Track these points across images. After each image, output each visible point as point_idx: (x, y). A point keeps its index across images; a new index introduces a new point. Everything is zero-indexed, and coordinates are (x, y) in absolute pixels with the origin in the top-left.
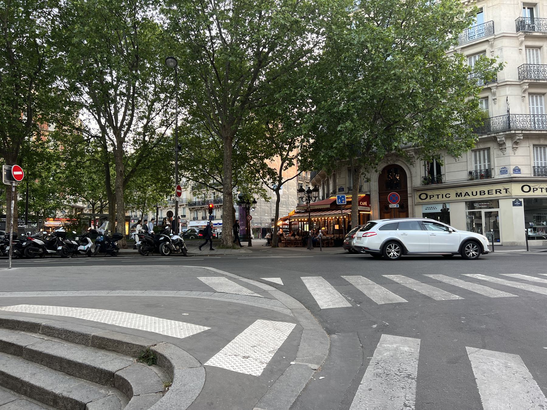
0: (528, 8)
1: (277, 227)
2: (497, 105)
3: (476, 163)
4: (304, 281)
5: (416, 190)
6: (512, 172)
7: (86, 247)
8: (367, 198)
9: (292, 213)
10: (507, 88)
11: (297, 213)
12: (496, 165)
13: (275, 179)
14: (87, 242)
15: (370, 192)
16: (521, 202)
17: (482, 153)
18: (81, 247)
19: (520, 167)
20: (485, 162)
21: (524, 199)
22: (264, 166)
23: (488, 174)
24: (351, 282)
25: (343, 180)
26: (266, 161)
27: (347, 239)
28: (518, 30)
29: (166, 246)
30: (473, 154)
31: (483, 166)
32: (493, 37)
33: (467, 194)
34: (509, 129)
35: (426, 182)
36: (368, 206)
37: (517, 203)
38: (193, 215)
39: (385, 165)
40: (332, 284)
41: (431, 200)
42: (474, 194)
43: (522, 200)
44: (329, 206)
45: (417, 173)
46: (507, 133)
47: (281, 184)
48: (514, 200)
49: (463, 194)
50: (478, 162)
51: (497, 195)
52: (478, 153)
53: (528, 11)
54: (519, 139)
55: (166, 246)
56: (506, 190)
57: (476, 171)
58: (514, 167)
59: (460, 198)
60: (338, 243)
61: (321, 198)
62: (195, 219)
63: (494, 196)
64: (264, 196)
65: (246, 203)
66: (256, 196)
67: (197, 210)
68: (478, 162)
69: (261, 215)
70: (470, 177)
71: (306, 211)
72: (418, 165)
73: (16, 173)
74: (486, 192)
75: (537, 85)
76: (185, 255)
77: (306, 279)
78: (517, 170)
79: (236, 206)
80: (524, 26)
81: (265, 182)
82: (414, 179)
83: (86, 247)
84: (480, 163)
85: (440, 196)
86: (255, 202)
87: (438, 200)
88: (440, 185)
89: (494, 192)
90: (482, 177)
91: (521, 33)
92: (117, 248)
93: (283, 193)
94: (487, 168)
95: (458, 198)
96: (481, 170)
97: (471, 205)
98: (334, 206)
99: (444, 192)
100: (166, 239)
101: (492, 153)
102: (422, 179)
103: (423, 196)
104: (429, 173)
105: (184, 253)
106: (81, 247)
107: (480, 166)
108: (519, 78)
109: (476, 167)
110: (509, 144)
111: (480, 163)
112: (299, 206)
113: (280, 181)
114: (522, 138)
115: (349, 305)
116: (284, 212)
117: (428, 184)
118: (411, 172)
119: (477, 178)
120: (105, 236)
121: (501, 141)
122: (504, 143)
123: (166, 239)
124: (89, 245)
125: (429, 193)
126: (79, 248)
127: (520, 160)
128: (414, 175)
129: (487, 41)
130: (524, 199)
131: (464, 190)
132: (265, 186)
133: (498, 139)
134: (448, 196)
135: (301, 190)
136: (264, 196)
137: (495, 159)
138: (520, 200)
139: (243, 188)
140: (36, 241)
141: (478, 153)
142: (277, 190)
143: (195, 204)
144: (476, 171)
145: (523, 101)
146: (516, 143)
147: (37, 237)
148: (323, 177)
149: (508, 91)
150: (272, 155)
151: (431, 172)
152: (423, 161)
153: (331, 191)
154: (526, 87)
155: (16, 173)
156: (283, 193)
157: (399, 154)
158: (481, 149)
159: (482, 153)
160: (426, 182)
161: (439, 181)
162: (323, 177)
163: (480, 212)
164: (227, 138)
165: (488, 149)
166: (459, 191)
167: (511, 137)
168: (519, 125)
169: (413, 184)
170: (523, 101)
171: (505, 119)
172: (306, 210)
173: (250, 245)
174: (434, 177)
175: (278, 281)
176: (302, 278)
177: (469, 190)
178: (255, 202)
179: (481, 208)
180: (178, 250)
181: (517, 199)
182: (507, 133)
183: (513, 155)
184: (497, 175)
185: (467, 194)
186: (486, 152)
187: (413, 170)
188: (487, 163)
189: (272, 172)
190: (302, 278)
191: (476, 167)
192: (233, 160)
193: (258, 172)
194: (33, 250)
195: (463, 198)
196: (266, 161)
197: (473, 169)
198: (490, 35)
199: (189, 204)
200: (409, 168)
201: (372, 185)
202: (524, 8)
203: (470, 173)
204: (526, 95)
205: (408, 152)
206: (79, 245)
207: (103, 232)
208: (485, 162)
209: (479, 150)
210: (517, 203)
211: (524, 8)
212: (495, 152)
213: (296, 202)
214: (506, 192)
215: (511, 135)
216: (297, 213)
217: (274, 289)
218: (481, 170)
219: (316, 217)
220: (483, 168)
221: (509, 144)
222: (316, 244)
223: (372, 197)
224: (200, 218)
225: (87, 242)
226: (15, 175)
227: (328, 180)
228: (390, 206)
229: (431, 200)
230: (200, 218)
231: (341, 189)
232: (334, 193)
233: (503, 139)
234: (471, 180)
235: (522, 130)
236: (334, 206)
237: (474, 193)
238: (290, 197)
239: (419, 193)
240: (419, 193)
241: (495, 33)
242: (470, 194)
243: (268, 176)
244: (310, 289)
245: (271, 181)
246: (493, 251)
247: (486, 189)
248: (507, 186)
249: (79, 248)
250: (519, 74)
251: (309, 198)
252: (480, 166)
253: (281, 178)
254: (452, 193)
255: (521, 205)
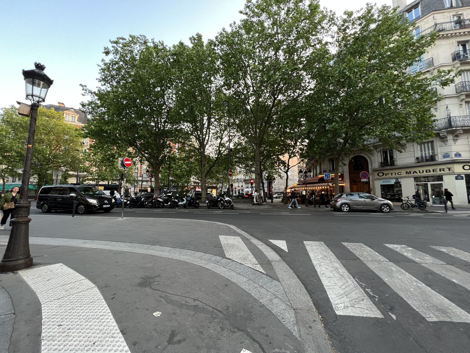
0: (462, 45)
1: (286, 192)
2: (438, 112)
3: (421, 151)
4: (308, 248)
5: (375, 170)
6: (454, 156)
7: (183, 203)
8: (342, 176)
9: (295, 185)
10: (447, 100)
11: (298, 185)
12: (439, 152)
13: (285, 166)
14: (184, 201)
15: (343, 172)
16: (462, 177)
17: (426, 145)
18: (180, 203)
19: (460, 153)
20: (429, 150)
21: (465, 175)
22: (279, 159)
23: (432, 158)
24: (357, 253)
25: (326, 165)
26: (281, 157)
27: (333, 202)
28: (454, 59)
29: (221, 204)
30: (419, 147)
31: (428, 153)
32: (433, 67)
33: (415, 172)
34: (450, 126)
35: (383, 165)
36: (342, 180)
37: (459, 178)
38: (246, 186)
39: (353, 156)
40: (338, 258)
41: (386, 177)
42: (421, 172)
43: (464, 176)
44: (317, 181)
45: (376, 160)
46: (449, 129)
47: (288, 169)
48: (456, 176)
49: (412, 173)
50: (423, 151)
51: (440, 173)
52: (423, 146)
53: (461, 48)
54: (459, 133)
55: (221, 204)
56: (449, 169)
57: (422, 157)
58: (455, 153)
59: (410, 175)
60: (327, 203)
61: (312, 176)
62: (247, 187)
63: (438, 173)
64: (280, 176)
65: (270, 180)
66: (275, 176)
67: (248, 183)
68: (423, 151)
69: (278, 185)
70: (417, 161)
71: (304, 184)
72: (376, 155)
73: (126, 162)
74: (432, 171)
75: (469, 96)
76: (232, 209)
77: (309, 245)
78: (458, 155)
79: (265, 181)
80: (460, 57)
81: (280, 168)
82: (373, 164)
83: (183, 203)
84: (425, 151)
85: (394, 174)
86: (274, 179)
87: (392, 176)
88: (393, 167)
89: (438, 170)
90: (427, 160)
91: (457, 62)
92: (198, 204)
93: (291, 172)
94: (431, 154)
95: (407, 175)
96: (426, 157)
97: (416, 179)
98: (322, 180)
99: (397, 171)
100: (222, 200)
101: (435, 144)
102: (380, 164)
103: (381, 174)
104: (384, 159)
105: (232, 208)
106: (180, 203)
107: (425, 154)
108: (457, 92)
109: (422, 154)
110: (450, 137)
111: (425, 151)
112: (299, 181)
113: (288, 167)
114: (462, 132)
115: (379, 315)
116: (291, 184)
117: (384, 166)
118: (371, 160)
119: (423, 161)
120: (191, 197)
121: (443, 135)
122: (446, 137)
123: (222, 200)
124: (185, 202)
125: (385, 172)
126: (179, 204)
127: (461, 147)
128: (373, 161)
129: (428, 71)
130: (465, 175)
131: (412, 170)
132: (280, 170)
133: (441, 135)
134: (399, 174)
135: (300, 172)
136: (280, 176)
137: (439, 148)
138: (462, 175)
139: (269, 172)
140: (159, 199)
141: (423, 146)
142: (286, 172)
143: (247, 180)
144: (422, 157)
145: (461, 107)
146: (457, 136)
147: (160, 198)
148: (313, 165)
149: (447, 102)
150: (283, 154)
151: (386, 159)
152: (380, 153)
153: (318, 172)
154: (464, 97)
155: (126, 162)
156: (291, 172)
157: (365, 148)
158: (426, 142)
159: (426, 145)
160: (383, 165)
161: (393, 164)
162: (313, 165)
163: (427, 184)
164: (257, 144)
165: (432, 142)
166: (408, 170)
167: (452, 132)
168: (459, 124)
169: (373, 167)
170: (461, 107)
171: (446, 120)
172: (303, 183)
173: (272, 202)
174: (388, 163)
175: (282, 244)
176: (305, 242)
177: (417, 170)
178: (274, 179)
179: (428, 181)
180: (228, 206)
181: (459, 175)
182: (449, 129)
183: (454, 144)
184: (440, 158)
185: (415, 172)
186: (430, 144)
187: (372, 158)
188: (430, 151)
189: (284, 163)
190: (305, 242)
191: (422, 154)
192: (262, 156)
193: (276, 162)
194: (158, 204)
195: (412, 174)
196: (281, 157)
197: (419, 155)
198: (430, 67)
199: (240, 180)
200: (369, 157)
201: (345, 169)
202: (458, 45)
203: (417, 158)
204: (463, 103)
205: (369, 147)
206: (179, 202)
207: (191, 195)
208: (429, 150)
209: (424, 143)
210: (459, 178)
211: (458, 45)
212: (437, 143)
213: (298, 179)
214: (449, 170)
215: (452, 130)
216: (298, 185)
217: (278, 258)
218: (426, 157)
219: (310, 188)
220: (427, 155)
221: (450, 137)
222: (310, 203)
223: (344, 175)
224: (249, 187)
225: (184, 201)
226: (126, 164)
227: (316, 166)
228: (362, 180)
229: (386, 177)
230: (249, 187)
231: (325, 171)
232: (320, 173)
233: (446, 134)
234: (418, 163)
235: (462, 127)
236: (322, 180)
237: (422, 172)
238: (294, 177)
239: (462, 165)
240: (462, 165)
241: (435, 65)
242: (418, 172)
243: (282, 165)
244: (315, 262)
245: (283, 167)
246: (446, 212)
247: (431, 168)
248: (449, 166)
249: (179, 204)
250: (456, 89)
251: (306, 176)
252: (425, 154)
253: (288, 165)
254: (403, 172)
255: (462, 179)
